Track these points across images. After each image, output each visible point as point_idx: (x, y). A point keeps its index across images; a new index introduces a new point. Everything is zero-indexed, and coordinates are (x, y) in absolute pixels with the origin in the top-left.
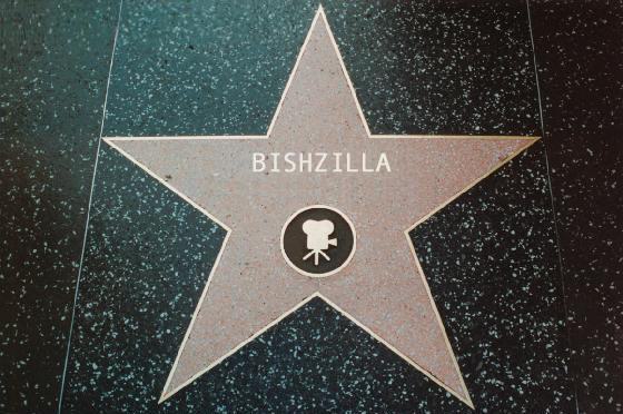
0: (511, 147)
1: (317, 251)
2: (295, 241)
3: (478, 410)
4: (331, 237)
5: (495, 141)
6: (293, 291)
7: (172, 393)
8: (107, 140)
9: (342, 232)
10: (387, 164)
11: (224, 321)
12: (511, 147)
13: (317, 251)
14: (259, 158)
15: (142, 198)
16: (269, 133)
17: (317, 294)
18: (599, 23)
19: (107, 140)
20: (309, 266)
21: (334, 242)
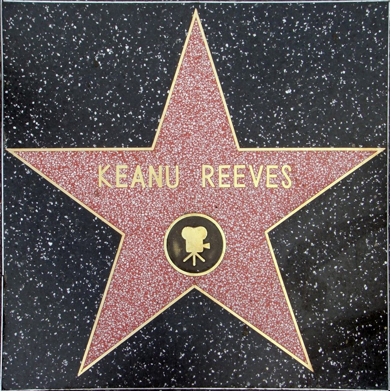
2: (176, 238)
3: (321, 374)
4: (205, 242)
9: (214, 237)
17: (123, 235)
20: (188, 267)
21: (208, 246)
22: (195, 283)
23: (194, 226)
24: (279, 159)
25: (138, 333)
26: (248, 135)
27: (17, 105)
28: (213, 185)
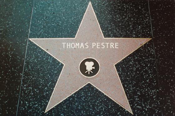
0: (143, 41)
1: (89, 70)
2: (83, 68)
3: (134, 115)
4: (93, 66)
5: (139, 39)
6: (82, 82)
7: (48, 110)
8: (30, 39)
9: (96, 65)
10: (83, 46)
11: (63, 90)
12: (143, 41)
13: (89, 70)
14: (112, 44)
15: (40, 55)
16: (75, 37)
18: (168, 6)
19: (30, 39)
20: (87, 74)
21: (94, 68)
22: (89, 81)
23: (89, 61)
24: (116, 41)
25: (84, 15)
26: (107, 35)
27: (7, 82)
28: (113, 48)
